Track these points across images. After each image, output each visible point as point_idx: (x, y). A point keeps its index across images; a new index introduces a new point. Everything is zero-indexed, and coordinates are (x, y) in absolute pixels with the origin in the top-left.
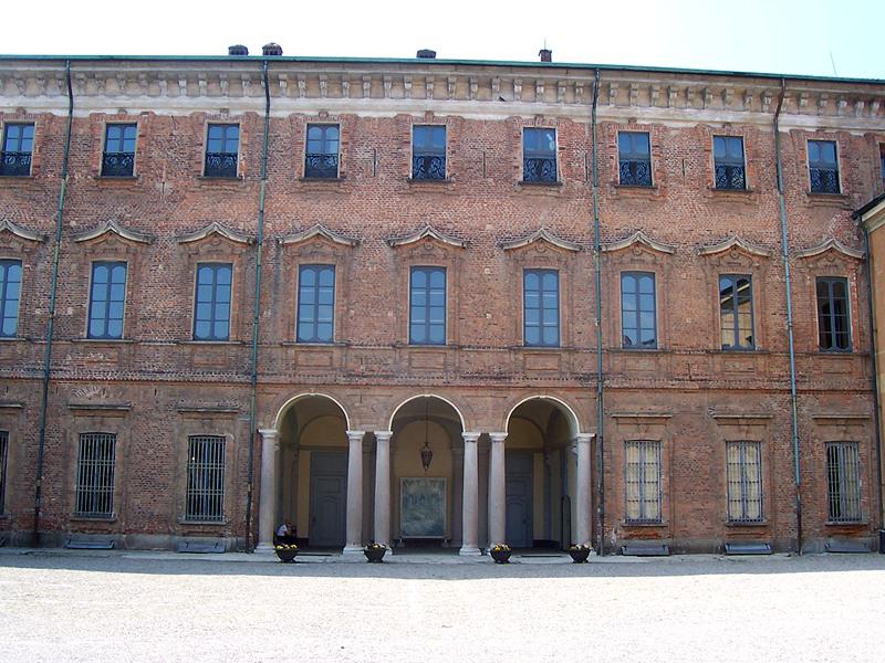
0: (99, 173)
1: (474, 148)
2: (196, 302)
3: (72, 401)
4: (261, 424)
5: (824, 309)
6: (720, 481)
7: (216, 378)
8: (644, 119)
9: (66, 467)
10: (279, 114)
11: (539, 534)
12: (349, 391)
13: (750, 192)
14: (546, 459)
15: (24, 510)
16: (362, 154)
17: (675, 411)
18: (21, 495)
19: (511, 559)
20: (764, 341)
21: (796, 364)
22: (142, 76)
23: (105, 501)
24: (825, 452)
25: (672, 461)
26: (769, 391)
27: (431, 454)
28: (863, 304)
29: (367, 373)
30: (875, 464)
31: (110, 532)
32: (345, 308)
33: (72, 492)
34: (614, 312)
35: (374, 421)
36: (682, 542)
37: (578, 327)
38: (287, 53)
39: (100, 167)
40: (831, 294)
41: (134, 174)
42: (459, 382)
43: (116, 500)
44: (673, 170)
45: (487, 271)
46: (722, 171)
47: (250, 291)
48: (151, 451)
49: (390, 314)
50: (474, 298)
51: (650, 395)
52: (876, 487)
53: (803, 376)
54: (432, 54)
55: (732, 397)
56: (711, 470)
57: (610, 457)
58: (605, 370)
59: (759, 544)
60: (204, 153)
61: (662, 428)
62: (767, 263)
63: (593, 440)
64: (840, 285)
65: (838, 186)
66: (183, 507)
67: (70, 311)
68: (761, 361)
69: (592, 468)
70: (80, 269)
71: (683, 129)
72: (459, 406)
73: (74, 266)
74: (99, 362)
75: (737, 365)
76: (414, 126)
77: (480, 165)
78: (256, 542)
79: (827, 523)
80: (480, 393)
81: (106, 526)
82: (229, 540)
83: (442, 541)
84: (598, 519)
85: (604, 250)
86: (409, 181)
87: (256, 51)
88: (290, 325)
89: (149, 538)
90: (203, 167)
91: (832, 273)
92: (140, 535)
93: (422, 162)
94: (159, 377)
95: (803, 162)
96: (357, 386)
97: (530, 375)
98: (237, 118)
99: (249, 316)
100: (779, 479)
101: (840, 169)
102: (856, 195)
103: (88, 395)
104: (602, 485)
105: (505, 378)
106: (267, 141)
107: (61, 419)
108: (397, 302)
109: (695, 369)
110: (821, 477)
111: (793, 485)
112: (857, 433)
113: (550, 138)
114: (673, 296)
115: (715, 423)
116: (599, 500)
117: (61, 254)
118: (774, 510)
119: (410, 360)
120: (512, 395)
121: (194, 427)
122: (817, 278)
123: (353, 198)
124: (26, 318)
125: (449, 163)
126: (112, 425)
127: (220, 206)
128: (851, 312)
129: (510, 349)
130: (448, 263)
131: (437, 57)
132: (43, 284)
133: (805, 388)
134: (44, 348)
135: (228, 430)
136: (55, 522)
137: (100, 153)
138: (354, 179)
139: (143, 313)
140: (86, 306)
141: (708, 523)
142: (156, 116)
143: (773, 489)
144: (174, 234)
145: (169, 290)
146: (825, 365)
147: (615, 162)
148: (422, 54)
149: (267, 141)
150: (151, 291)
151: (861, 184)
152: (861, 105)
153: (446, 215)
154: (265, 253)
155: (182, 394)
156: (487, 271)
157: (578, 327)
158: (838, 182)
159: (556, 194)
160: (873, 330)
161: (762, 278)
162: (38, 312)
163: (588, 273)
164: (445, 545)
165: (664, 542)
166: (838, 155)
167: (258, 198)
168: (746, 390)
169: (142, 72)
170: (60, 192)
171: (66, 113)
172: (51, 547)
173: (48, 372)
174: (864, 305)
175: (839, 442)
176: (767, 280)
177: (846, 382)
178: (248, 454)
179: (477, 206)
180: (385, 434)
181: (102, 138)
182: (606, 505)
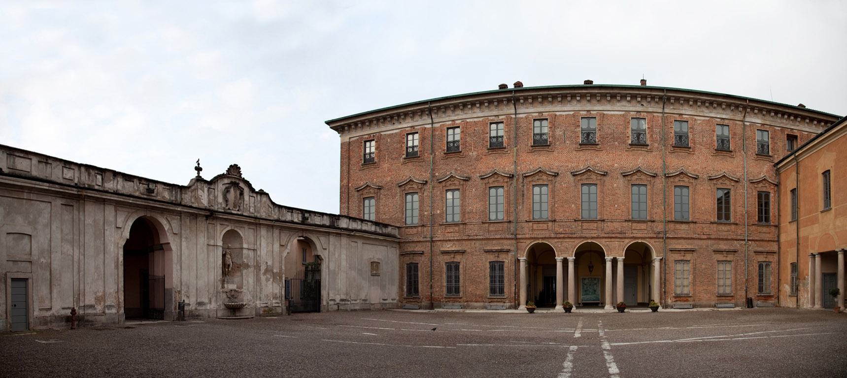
0: (446, 151)
1: (609, 128)
2: (489, 204)
3: (442, 249)
4: (519, 255)
5: (760, 205)
6: (715, 278)
7: (498, 237)
8: (686, 115)
9: (441, 276)
10: (521, 116)
11: (640, 300)
12: (556, 240)
13: (731, 152)
14: (643, 268)
15: (427, 294)
16: (559, 132)
17: (696, 247)
18: (425, 288)
19: (626, 310)
20: (735, 218)
21: (747, 228)
22: (460, 105)
23: (457, 290)
24: (758, 266)
25: (695, 269)
26: (736, 240)
27: (593, 267)
28: (776, 204)
29: (563, 232)
30: (777, 271)
31: (460, 302)
32: (553, 204)
33: (444, 286)
34: (671, 204)
35: (567, 253)
36: (698, 303)
37: (655, 210)
38: (525, 86)
39: (446, 148)
40: (763, 199)
41: (460, 150)
42: (603, 235)
43: (461, 289)
44: (698, 139)
45: (615, 185)
46: (720, 141)
47: (512, 198)
48: (474, 269)
49: (573, 206)
50: (609, 198)
51: (685, 241)
52: (777, 280)
53: (751, 234)
54: (591, 82)
55: (721, 242)
56: (711, 273)
57: (669, 268)
58: (667, 230)
59: (730, 304)
60: (489, 137)
61: (691, 255)
62: (737, 184)
63: (661, 260)
64: (767, 195)
65: (769, 151)
66: (488, 291)
67: (438, 212)
68: (733, 227)
69: (661, 272)
70: (441, 193)
71: (703, 120)
72: (604, 245)
73: (439, 192)
74: (451, 232)
75: (723, 229)
76: (582, 118)
77: (612, 136)
78: (519, 305)
79: (757, 295)
80: (613, 240)
81: (458, 299)
82: (508, 304)
83: (599, 303)
84: (664, 294)
85: (667, 175)
86: (580, 145)
87: (511, 86)
88: (530, 212)
89: (476, 304)
90: (489, 143)
91: (764, 189)
92: (472, 303)
93: (585, 135)
94: (475, 238)
95: (755, 139)
96: (560, 238)
97: (634, 232)
98: (502, 119)
99: (512, 209)
100: (738, 276)
101: (770, 144)
102: (776, 156)
103: (448, 246)
104: (665, 279)
105: (623, 233)
106: (517, 129)
107: (438, 257)
108: (576, 200)
109: (705, 230)
110: (756, 276)
111: (744, 280)
112: (770, 258)
113: (644, 123)
114: (697, 197)
115: (713, 253)
116: (663, 286)
117: (433, 187)
118: (736, 289)
119: (582, 226)
120: (627, 241)
121: (492, 258)
122: (758, 191)
123: (555, 154)
124: (421, 216)
125: (597, 135)
126: (458, 258)
127: (497, 161)
128: (771, 207)
129: (626, 221)
130: (598, 182)
131: (594, 84)
132: (427, 202)
133: (751, 238)
134: (429, 228)
135: (506, 259)
136: (438, 298)
137: (445, 142)
138: (555, 144)
139: (468, 210)
140: (445, 209)
141: (709, 295)
142: (467, 122)
143: (736, 281)
144: (478, 175)
145: (478, 200)
146: (760, 229)
147: (673, 135)
148: (587, 82)
149: (517, 129)
150: (470, 201)
151: (778, 151)
152: (780, 115)
153: (597, 160)
154: (517, 180)
155: (485, 244)
156: (615, 185)
157: (655, 210)
158: (768, 150)
159: (646, 150)
160: (779, 215)
161: (735, 191)
162: (426, 213)
163: (660, 186)
164: (600, 305)
165: (691, 303)
166: (770, 137)
167: (513, 156)
168: (727, 239)
169: (460, 103)
170: (430, 161)
171: (430, 126)
172: (438, 308)
173: (432, 238)
174: (777, 204)
175: (764, 262)
176: (737, 191)
177: (767, 237)
178: (514, 268)
179: (611, 155)
180: (571, 258)
181: (446, 135)
182: (666, 288)
